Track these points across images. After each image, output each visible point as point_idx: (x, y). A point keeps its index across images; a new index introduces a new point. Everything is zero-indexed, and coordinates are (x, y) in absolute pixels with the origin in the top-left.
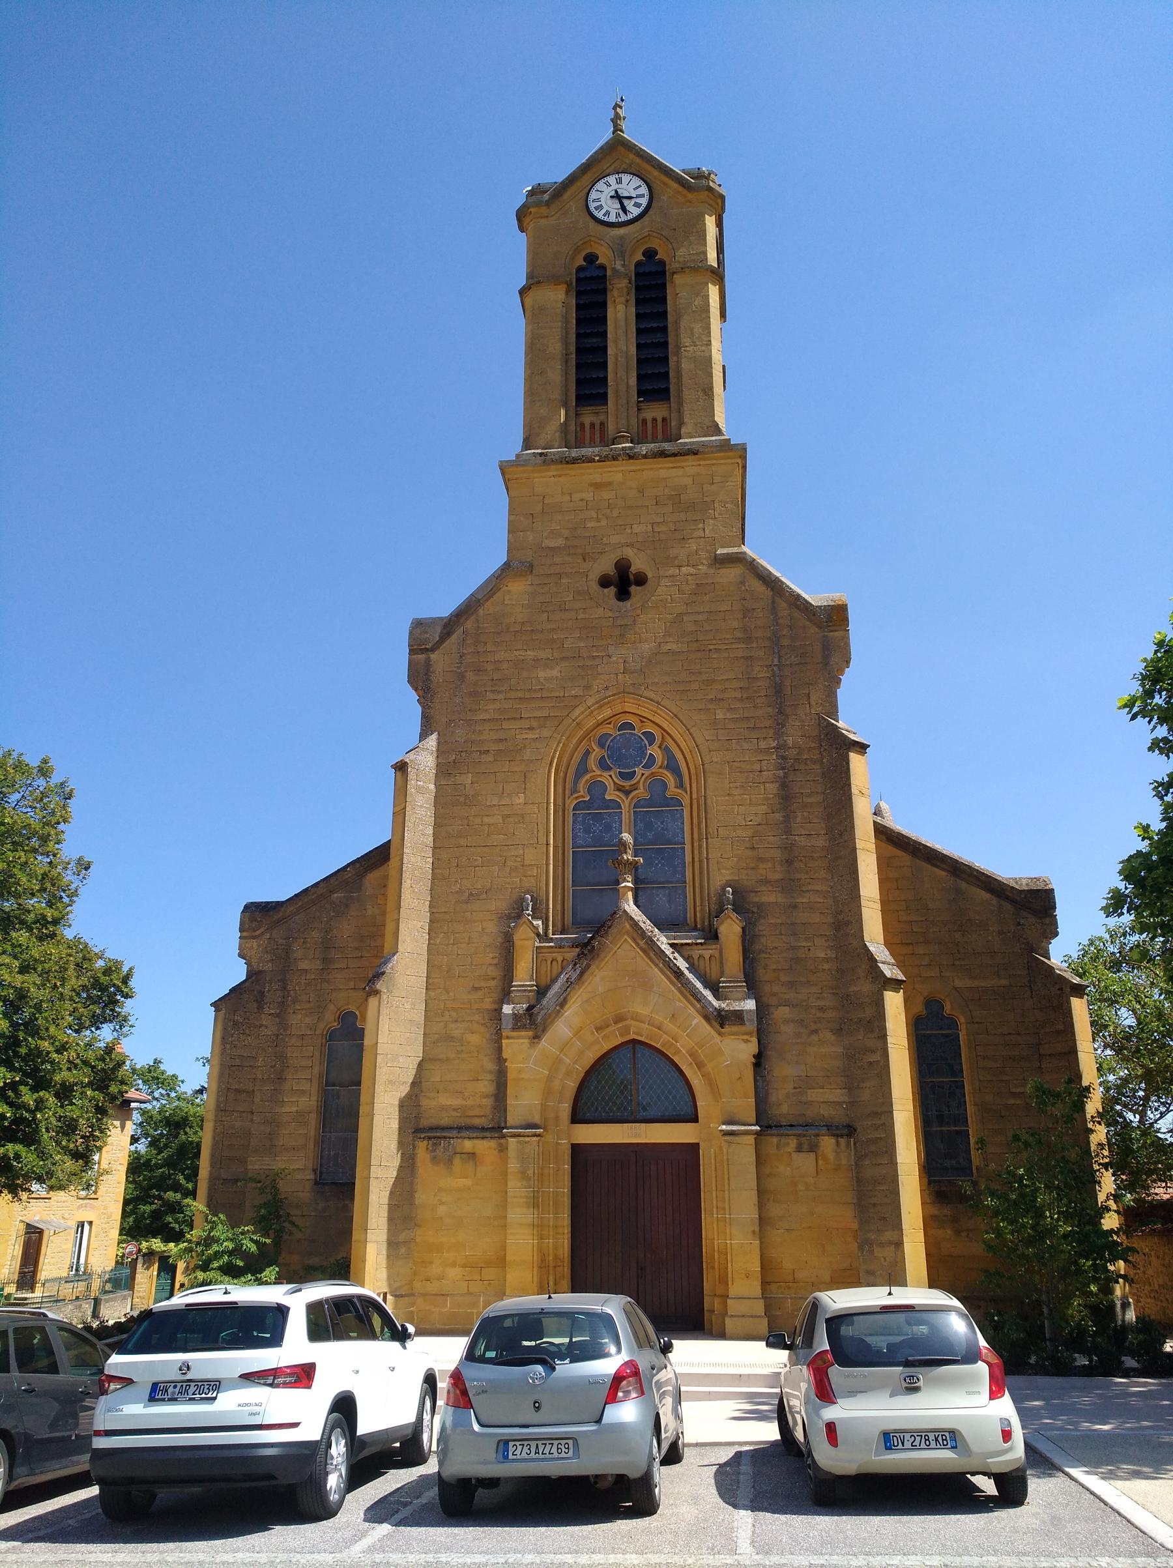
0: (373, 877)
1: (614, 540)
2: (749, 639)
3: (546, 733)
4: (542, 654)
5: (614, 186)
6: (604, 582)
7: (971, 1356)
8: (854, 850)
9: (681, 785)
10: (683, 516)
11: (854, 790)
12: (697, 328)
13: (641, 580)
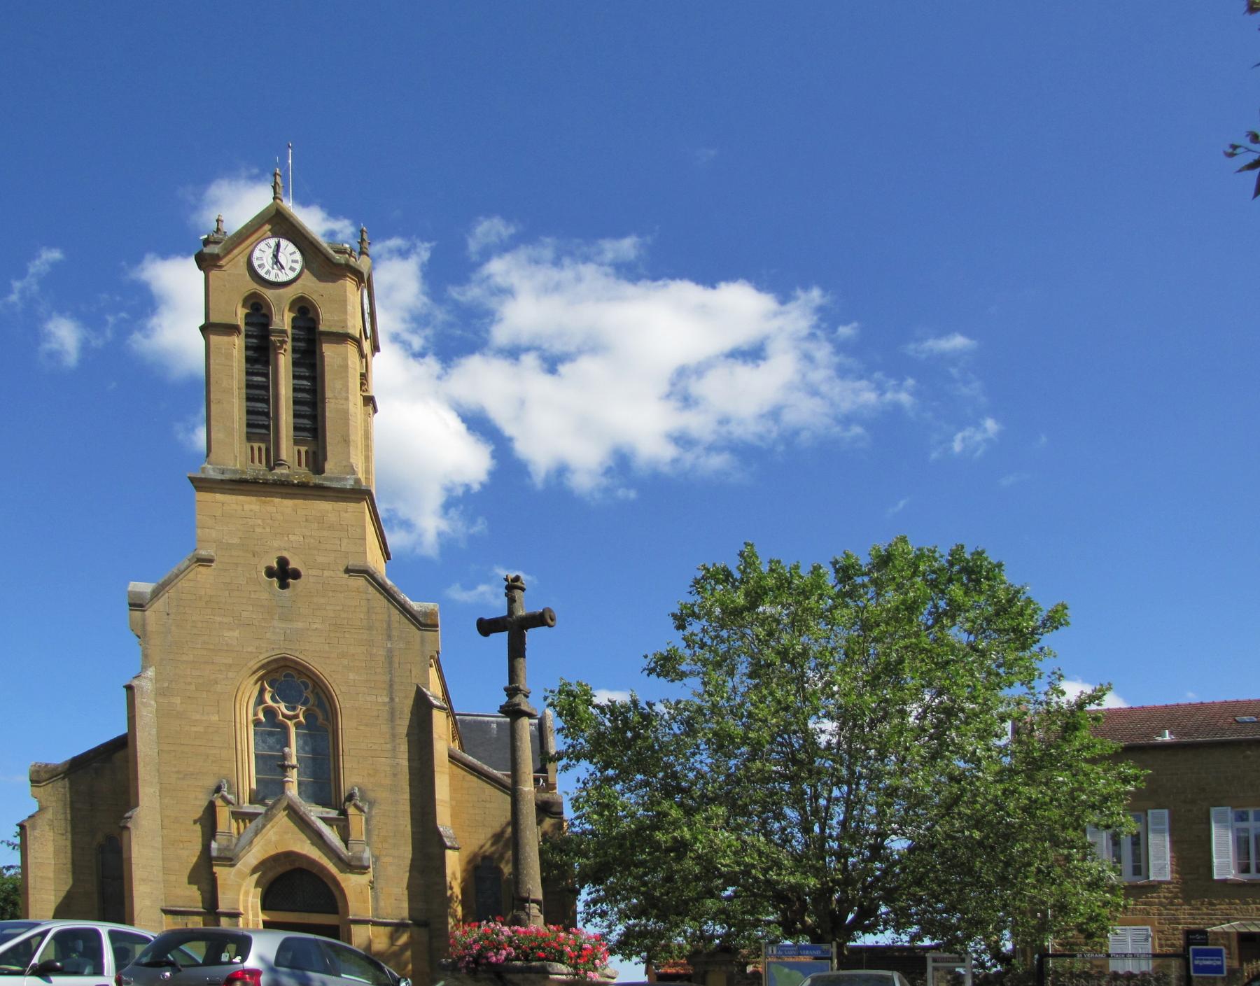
0: (119, 755)
1: (276, 544)
2: (370, 628)
3: (231, 675)
4: (225, 620)
5: (273, 272)
6: (270, 573)
7: (392, 944)
8: (433, 772)
9: (327, 719)
10: (325, 533)
11: (435, 736)
12: (338, 385)
13: (296, 575)
